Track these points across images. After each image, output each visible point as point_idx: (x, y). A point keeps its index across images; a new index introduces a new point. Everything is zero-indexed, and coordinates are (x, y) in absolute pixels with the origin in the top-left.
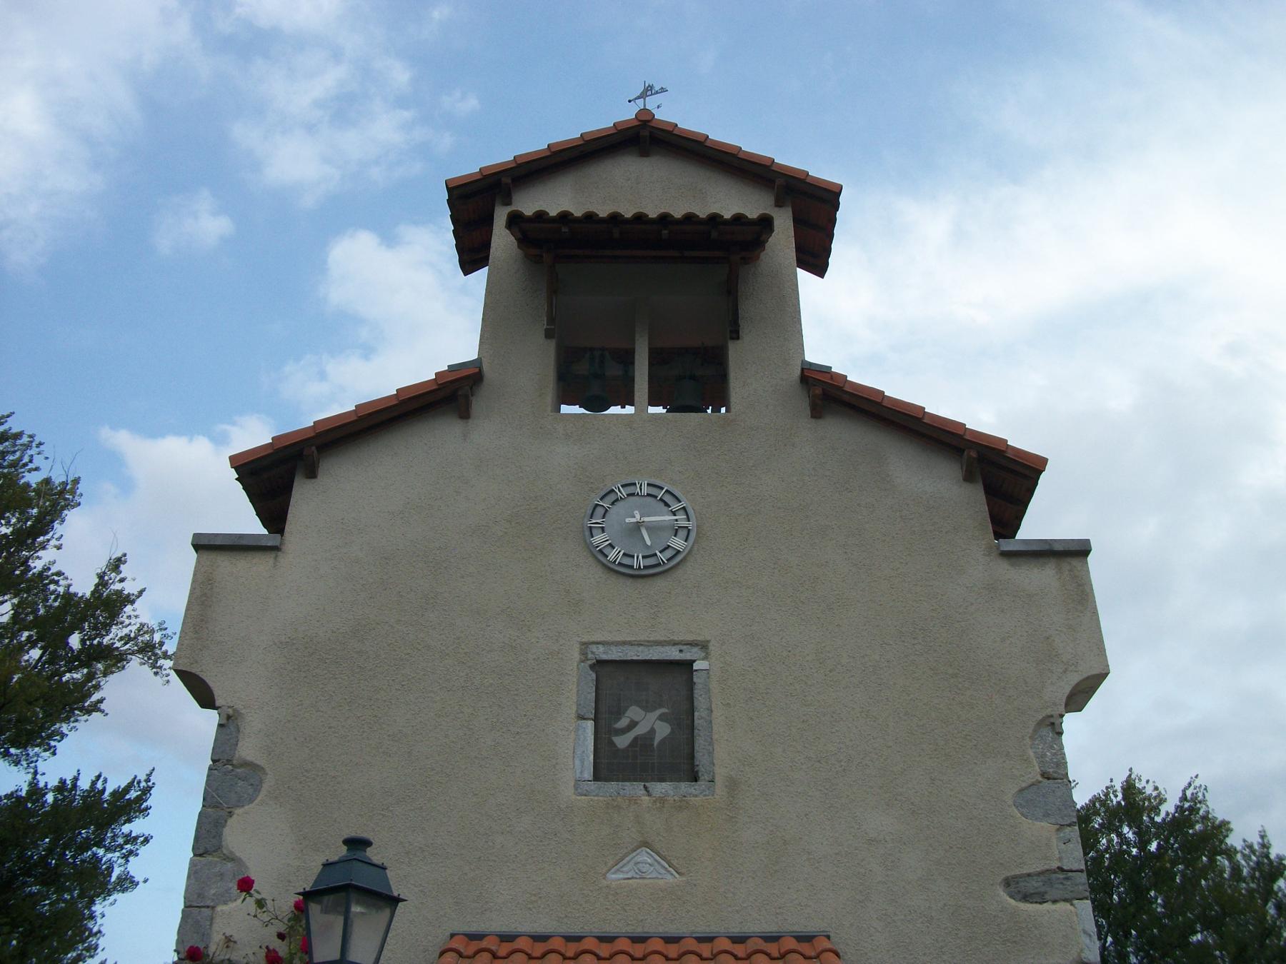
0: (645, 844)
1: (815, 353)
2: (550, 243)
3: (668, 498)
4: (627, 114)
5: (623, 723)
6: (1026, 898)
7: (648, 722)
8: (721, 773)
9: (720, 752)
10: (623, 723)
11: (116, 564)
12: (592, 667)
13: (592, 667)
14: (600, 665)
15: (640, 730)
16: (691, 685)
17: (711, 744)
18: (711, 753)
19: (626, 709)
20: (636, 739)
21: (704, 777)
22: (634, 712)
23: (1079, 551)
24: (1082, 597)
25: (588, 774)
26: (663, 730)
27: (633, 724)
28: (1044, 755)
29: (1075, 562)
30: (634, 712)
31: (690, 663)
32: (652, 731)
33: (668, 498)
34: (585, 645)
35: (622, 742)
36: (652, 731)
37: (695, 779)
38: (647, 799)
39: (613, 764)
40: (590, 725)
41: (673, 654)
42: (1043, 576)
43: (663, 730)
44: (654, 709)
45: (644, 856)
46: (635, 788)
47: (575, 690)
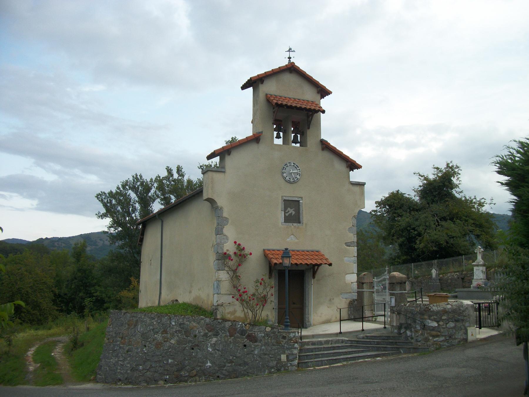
1: (323, 137)
6: (348, 246)
7: (291, 211)
8: (304, 222)
10: (287, 211)
15: (290, 212)
16: (299, 205)
22: (289, 209)
23: (363, 184)
27: (289, 211)
30: (289, 209)
35: (287, 215)
37: (300, 223)
39: (288, 219)
41: (297, 199)
42: (357, 189)
43: (294, 213)
45: (292, 236)
47: (280, 205)
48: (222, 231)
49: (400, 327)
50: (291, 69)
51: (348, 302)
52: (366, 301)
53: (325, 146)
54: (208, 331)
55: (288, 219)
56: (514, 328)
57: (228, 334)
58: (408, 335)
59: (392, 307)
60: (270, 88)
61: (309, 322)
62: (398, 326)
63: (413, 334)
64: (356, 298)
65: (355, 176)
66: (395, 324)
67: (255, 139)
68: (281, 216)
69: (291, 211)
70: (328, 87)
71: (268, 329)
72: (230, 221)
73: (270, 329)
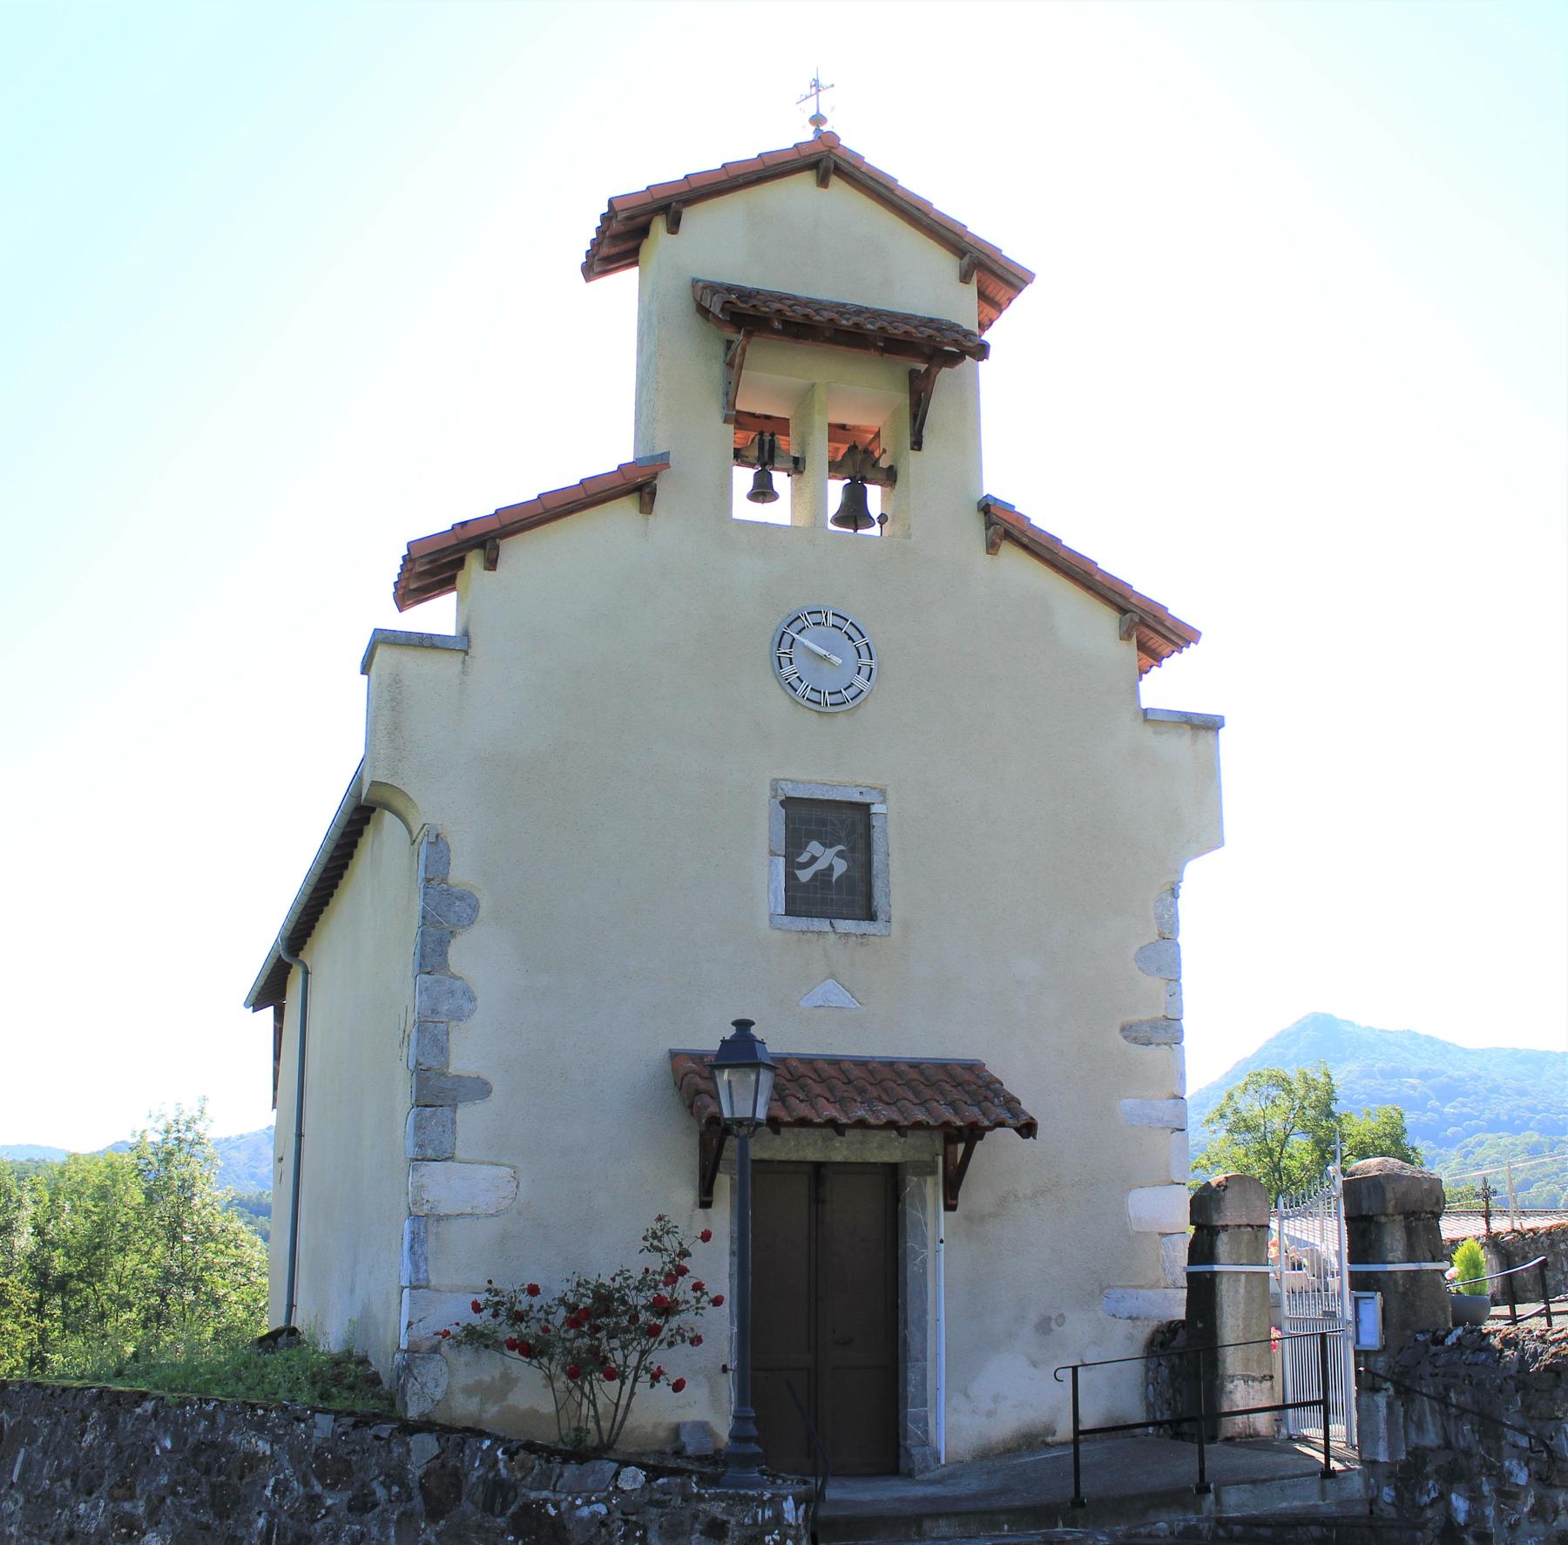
0: (832, 976)
1: (995, 484)
2: (742, 320)
3: (864, 651)
4: (807, 134)
5: (804, 858)
6: (1135, 1040)
7: (827, 858)
8: (896, 913)
9: (897, 896)
10: (804, 858)
11: (1028, 1129)
12: (782, 803)
13: (782, 803)
14: (788, 802)
15: (820, 865)
16: (868, 827)
17: (888, 886)
18: (888, 895)
19: (807, 844)
20: (816, 874)
21: (881, 916)
22: (814, 847)
23: (1209, 725)
24: (1209, 772)
25: (781, 910)
26: (840, 867)
27: (814, 859)
28: (1162, 917)
29: (1210, 735)
30: (814, 847)
31: (867, 806)
32: (831, 868)
33: (864, 651)
34: (776, 780)
35: (804, 876)
36: (831, 868)
37: (871, 917)
38: (833, 937)
39: (805, 899)
40: (782, 860)
41: (857, 798)
42: (1178, 745)
43: (840, 867)
44: (831, 846)
45: (831, 982)
46: (823, 925)
47: (767, 827)
48: (444, 954)
49: (1408, 1474)
50: (824, 162)
51: (1143, 1332)
52: (1231, 1324)
53: (1003, 527)
54: (325, 1486)
55: (805, 899)
56: (722, 1445)
57: (418, 1502)
58: (1461, 1518)
59: (1367, 1353)
60: (716, 246)
61: (925, 1443)
62: (1405, 1466)
63: (1490, 1511)
64: (1180, 1313)
65: (1168, 686)
66: (1383, 1457)
67: (637, 485)
68: (767, 880)
69: (827, 858)
70: (1180, 609)
71: (632, 1479)
72: (485, 904)
73: (641, 1475)
